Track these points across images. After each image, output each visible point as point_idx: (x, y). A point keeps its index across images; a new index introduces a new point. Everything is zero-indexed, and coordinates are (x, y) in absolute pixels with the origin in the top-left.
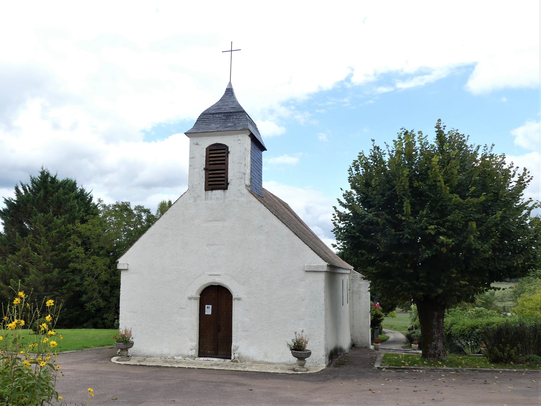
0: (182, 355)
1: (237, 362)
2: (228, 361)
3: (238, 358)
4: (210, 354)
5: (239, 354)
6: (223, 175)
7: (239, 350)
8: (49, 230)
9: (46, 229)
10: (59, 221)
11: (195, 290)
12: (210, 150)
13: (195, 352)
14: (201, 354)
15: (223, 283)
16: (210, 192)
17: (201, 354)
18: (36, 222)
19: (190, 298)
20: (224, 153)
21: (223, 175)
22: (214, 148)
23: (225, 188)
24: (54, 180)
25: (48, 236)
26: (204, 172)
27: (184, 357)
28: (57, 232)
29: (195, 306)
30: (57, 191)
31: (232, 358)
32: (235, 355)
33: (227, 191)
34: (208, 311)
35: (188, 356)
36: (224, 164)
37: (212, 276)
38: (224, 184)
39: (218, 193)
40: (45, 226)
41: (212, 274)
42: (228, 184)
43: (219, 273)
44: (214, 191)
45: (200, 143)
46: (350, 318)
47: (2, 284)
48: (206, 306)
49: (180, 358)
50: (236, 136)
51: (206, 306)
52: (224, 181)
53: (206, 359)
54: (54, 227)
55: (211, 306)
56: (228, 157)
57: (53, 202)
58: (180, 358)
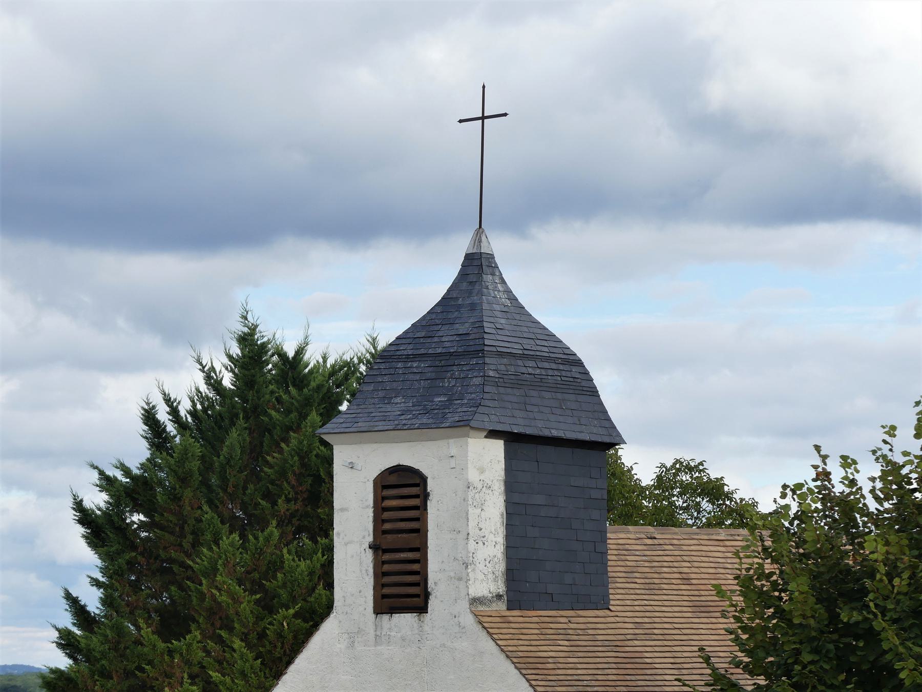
6: (416, 567)
8: (268, 605)
9: (257, 602)
10: (303, 565)
12: (385, 487)
16: (386, 617)
18: (213, 571)
20: (417, 496)
21: (416, 567)
22: (393, 479)
23: (422, 609)
24: (292, 366)
25: (262, 635)
26: (369, 556)
28: (296, 615)
30: (298, 429)
33: (427, 617)
36: (417, 531)
38: (418, 596)
39: (405, 620)
40: (256, 587)
42: (427, 595)
44: (396, 617)
45: (359, 464)
47: (809, 690)
50: (442, 443)
52: (417, 584)
54: (284, 595)
56: (426, 509)
57: (283, 474)
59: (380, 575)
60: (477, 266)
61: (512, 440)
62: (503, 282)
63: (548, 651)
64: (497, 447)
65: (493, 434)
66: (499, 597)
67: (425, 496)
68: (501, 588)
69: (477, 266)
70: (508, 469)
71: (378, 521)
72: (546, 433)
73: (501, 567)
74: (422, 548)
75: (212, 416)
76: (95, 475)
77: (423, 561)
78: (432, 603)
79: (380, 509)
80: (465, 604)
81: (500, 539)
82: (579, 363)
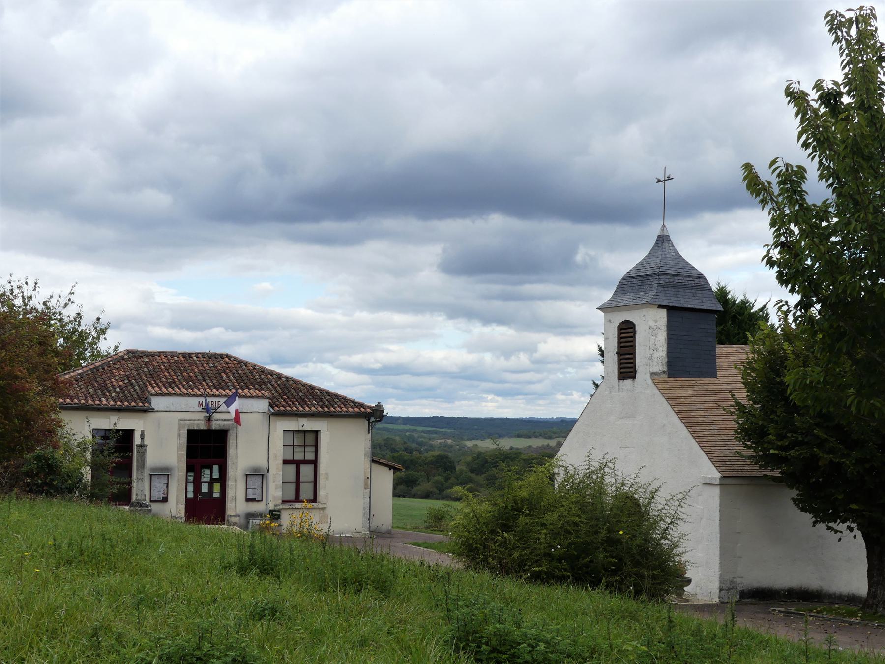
6: (632, 361)
21: (632, 361)
22: (624, 326)
23: (634, 378)
26: (616, 356)
39: (628, 382)
59: (620, 364)
60: (663, 240)
61: (670, 309)
62: (673, 246)
63: (683, 394)
64: (664, 313)
65: (660, 307)
66: (664, 372)
67: (635, 332)
68: (665, 369)
69: (663, 240)
70: (668, 321)
71: (619, 343)
72: (686, 306)
73: (665, 360)
74: (634, 353)
75: (803, 253)
76: (156, 409)
77: (634, 358)
78: (638, 375)
79: (620, 338)
80: (649, 375)
81: (665, 349)
82: (704, 278)
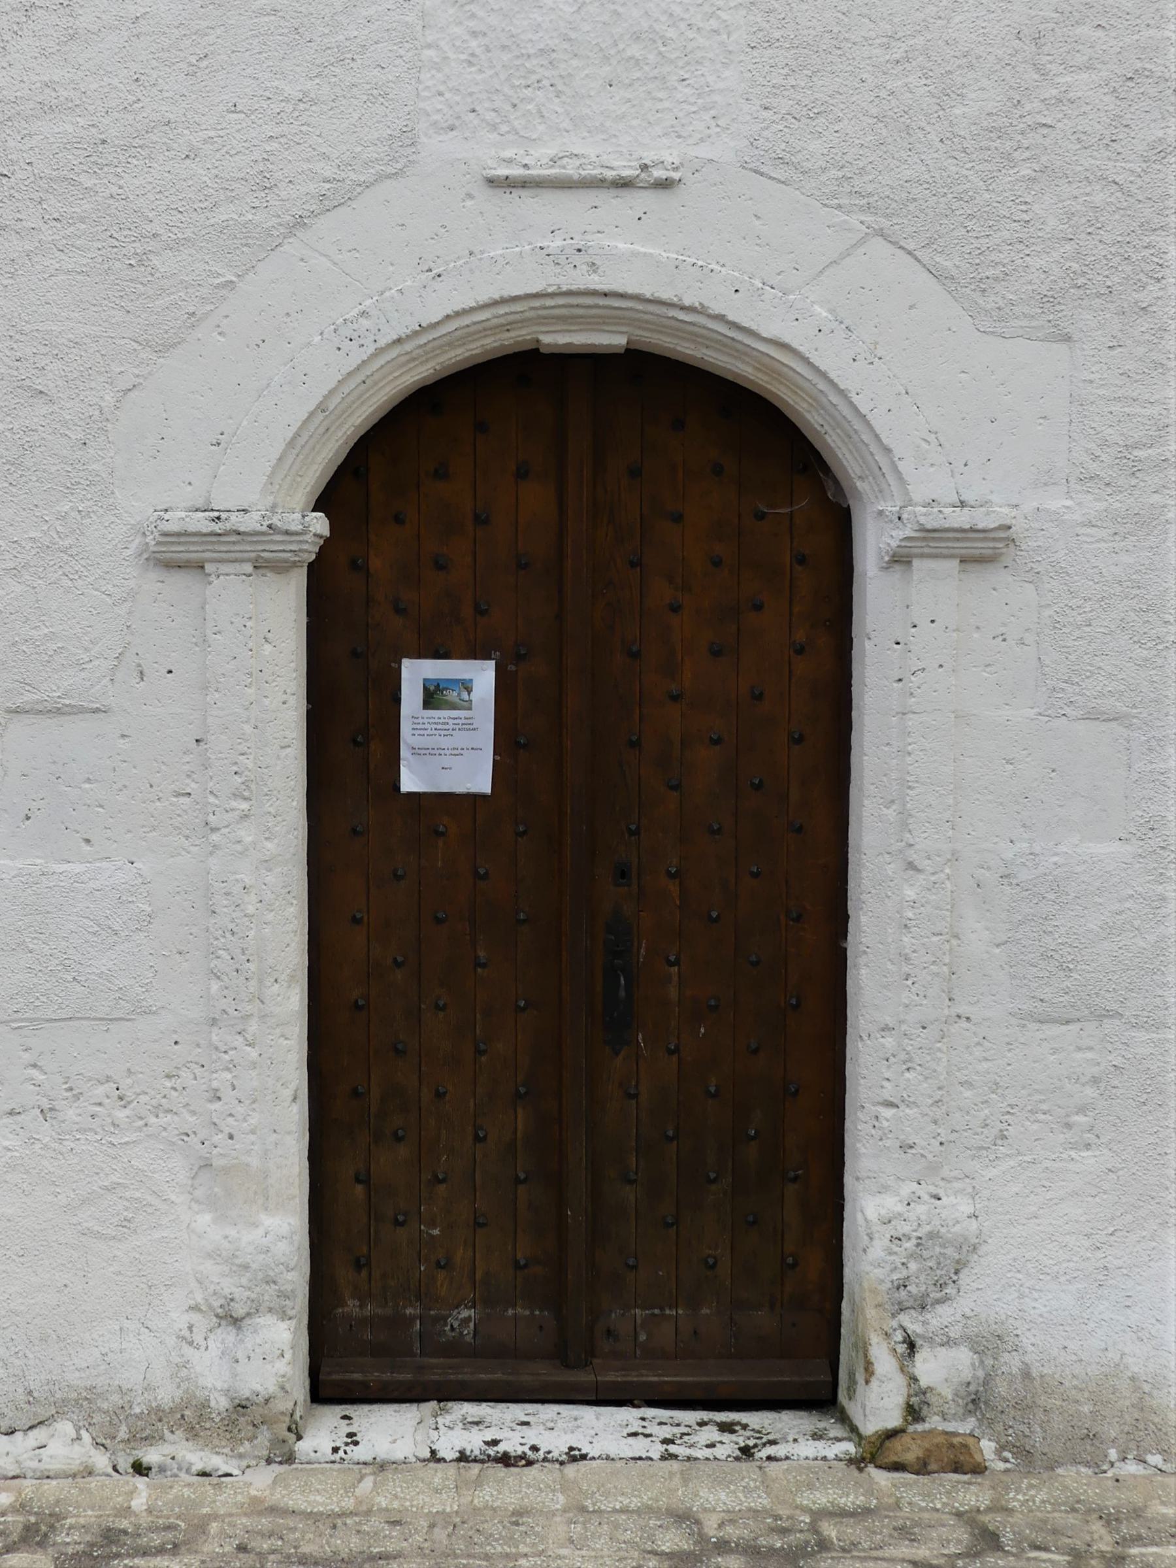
0: (81, 1405)
1: (961, 1461)
2: (796, 1439)
3: (975, 1401)
4: (486, 1350)
5: (988, 1343)
7: (978, 1298)
11: (259, 422)
13: (277, 1352)
14: (351, 1361)
15: (832, 357)
17: (351, 1361)
19: (182, 556)
27: (132, 1433)
29: (255, 654)
31: (878, 1404)
32: (932, 1368)
34: (448, 744)
35: (191, 1418)
37: (528, 204)
41: (538, 159)
43: (665, 154)
46: (321, 407)
48: (415, 673)
49: (63, 1446)
51: (415, 673)
53: (461, 1427)
55: (482, 677)
58: (63, 1446)
